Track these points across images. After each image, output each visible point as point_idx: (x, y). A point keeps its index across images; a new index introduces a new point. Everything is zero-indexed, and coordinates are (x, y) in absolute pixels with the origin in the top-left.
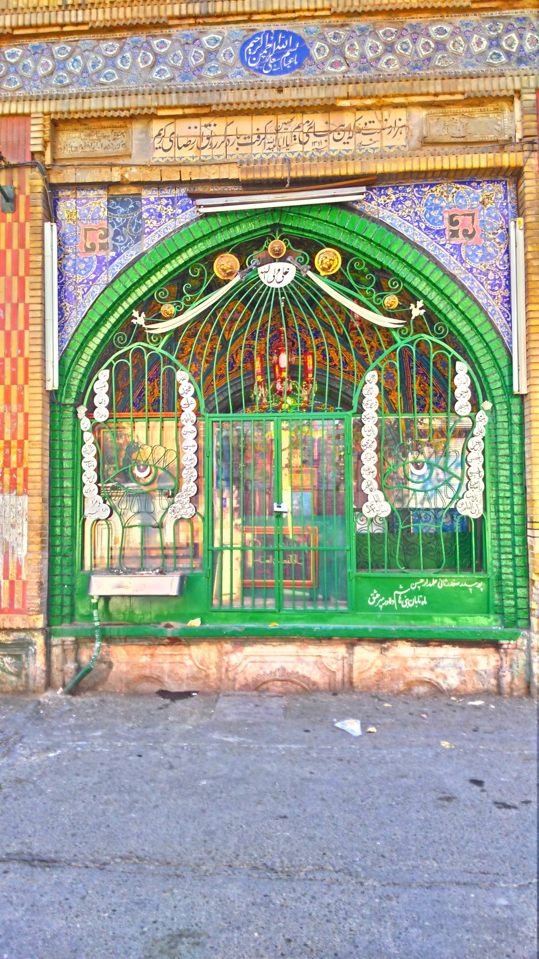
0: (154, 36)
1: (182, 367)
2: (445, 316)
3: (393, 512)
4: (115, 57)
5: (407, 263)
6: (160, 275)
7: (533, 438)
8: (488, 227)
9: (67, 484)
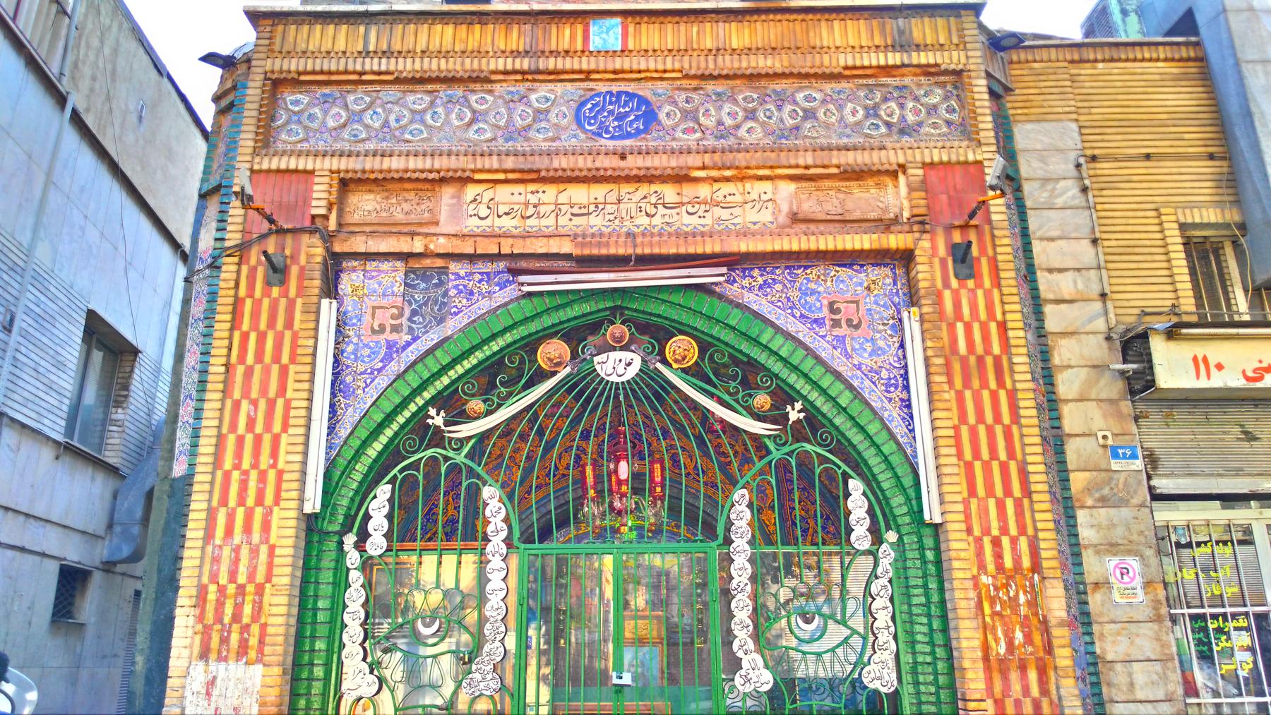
0: (473, 91)
1: (490, 481)
2: (831, 421)
3: (776, 683)
4: (424, 111)
5: (781, 357)
6: (467, 365)
7: (955, 583)
8: (876, 317)
9: (320, 645)
